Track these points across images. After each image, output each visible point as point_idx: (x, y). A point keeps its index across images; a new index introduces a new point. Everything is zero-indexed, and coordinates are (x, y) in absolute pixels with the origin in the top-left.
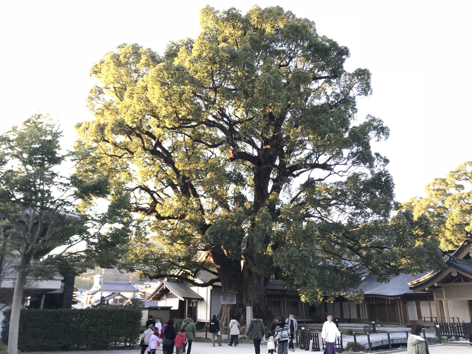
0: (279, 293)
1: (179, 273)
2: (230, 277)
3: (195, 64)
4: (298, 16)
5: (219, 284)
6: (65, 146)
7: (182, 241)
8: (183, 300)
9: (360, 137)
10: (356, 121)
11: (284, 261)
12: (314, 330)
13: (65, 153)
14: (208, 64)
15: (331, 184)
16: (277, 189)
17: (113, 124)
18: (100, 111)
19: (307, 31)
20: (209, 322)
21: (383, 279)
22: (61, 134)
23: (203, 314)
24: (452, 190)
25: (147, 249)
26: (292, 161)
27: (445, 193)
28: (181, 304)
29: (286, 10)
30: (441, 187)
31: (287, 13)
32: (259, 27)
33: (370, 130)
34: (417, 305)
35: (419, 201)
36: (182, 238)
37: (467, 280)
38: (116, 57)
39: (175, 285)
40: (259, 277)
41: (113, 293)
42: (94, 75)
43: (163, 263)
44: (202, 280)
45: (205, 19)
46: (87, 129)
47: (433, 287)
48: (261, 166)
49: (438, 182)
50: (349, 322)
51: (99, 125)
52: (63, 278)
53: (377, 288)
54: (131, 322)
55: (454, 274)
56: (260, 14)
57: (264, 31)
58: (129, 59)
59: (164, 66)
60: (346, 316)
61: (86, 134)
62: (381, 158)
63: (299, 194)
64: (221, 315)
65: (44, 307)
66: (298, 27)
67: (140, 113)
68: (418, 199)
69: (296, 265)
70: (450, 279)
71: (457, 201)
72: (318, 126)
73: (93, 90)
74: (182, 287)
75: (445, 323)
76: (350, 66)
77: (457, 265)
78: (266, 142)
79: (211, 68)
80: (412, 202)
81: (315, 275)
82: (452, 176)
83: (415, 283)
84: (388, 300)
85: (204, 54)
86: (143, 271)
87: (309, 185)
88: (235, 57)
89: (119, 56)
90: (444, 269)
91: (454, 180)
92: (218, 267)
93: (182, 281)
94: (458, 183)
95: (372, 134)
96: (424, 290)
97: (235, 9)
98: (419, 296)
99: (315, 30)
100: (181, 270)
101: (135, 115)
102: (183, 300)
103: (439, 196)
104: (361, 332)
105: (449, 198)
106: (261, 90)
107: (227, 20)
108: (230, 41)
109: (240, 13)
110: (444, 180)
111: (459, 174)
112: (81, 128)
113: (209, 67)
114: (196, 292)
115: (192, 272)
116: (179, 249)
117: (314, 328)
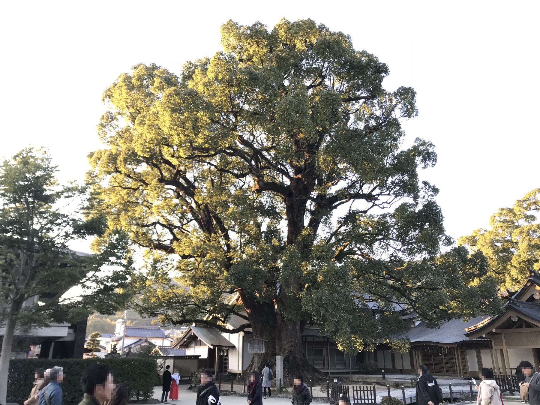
0: (321, 340)
1: (209, 317)
2: (263, 320)
3: (209, 88)
4: (332, 30)
5: (250, 330)
6: (61, 180)
7: (205, 282)
8: (212, 347)
9: (406, 164)
10: (405, 144)
11: (312, 305)
12: (359, 382)
13: (59, 189)
14: (226, 87)
15: (378, 216)
16: (314, 224)
17: (126, 154)
18: (113, 139)
19: (340, 47)
20: (241, 372)
21: (432, 324)
22: (57, 169)
23: (235, 364)
24: (522, 222)
25: (170, 290)
26: (333, 190)
27: (512, 225)
28: (211, 352)
29: (317, 24)
30: (508, 218)
31: (320, 26)
32: (289, 43)
33: (414, 156)
34: (477, 353)
35: (483, 235)
36: (205, 279)
37: (529, 325)
38: (127, 79)
39: (205, 331)
40: (294, 323)
41: (140, 340)
42: (107, 100)
43: (190, 306)
44: (233, 325)
45: (226, 35)
46: (99, 159)
47: (491, 333)
48: (294, 198)
49: (504, 212)
50: (402, 374)
51: (111, 154)
52: (70, 325)
53: (430, 336)
54: (144, 373)
55: (515, 319)
56: (290, 29)
57: (295, 45)
58: (142, 82)
59: (175, 90)
60: (398, 366)
61: (98, 165)
62: (430, 187)
63: (340, 228)
64: (252, 365)
65: (54, 357)
66: (329, 43)
67: (151, 142)
68: (482, 232)
69: (327, 310)
70: (509, 325)
71: (525, 234)
72: (349, 153)
73: (105, 117)
74: (212, 334)
75: (507, 376)
76: (389, 84)
77: (517, 308)
78: (298, 171)
79: (229, 91)
80: (476, 236)
81: (349, 321)
82: (520, 206)
83: (473, 329)
84: (444, 348)
85: (220, 77)
86: (166, 315)
87: (351, 217)
88: (255, 79)
89: (131, 78)
90: (502, 314)
91: (523, 210)
92: (248, 311)
93: (211, 326)
94: (529, 213)
95: (418, 160)
96: (481, 337)
97: (260, 24)
98: (476, 343)
99: (351, 45)
100: (210, 315)
101: (147, 144)
102: (212, 347)
103: (504, 228)
104: (409, 385)
105: (517, 231)
106: (282, 115)
107: (251, 36)
108: (254, 59)
109: (266, 28)
110: (511, 211)
111: (529, 202)
112: (93, 158)
113: (227, 90)
114: (228, 339)
115: (222, 316)
116: (203, 291)
117: (359, 380)
